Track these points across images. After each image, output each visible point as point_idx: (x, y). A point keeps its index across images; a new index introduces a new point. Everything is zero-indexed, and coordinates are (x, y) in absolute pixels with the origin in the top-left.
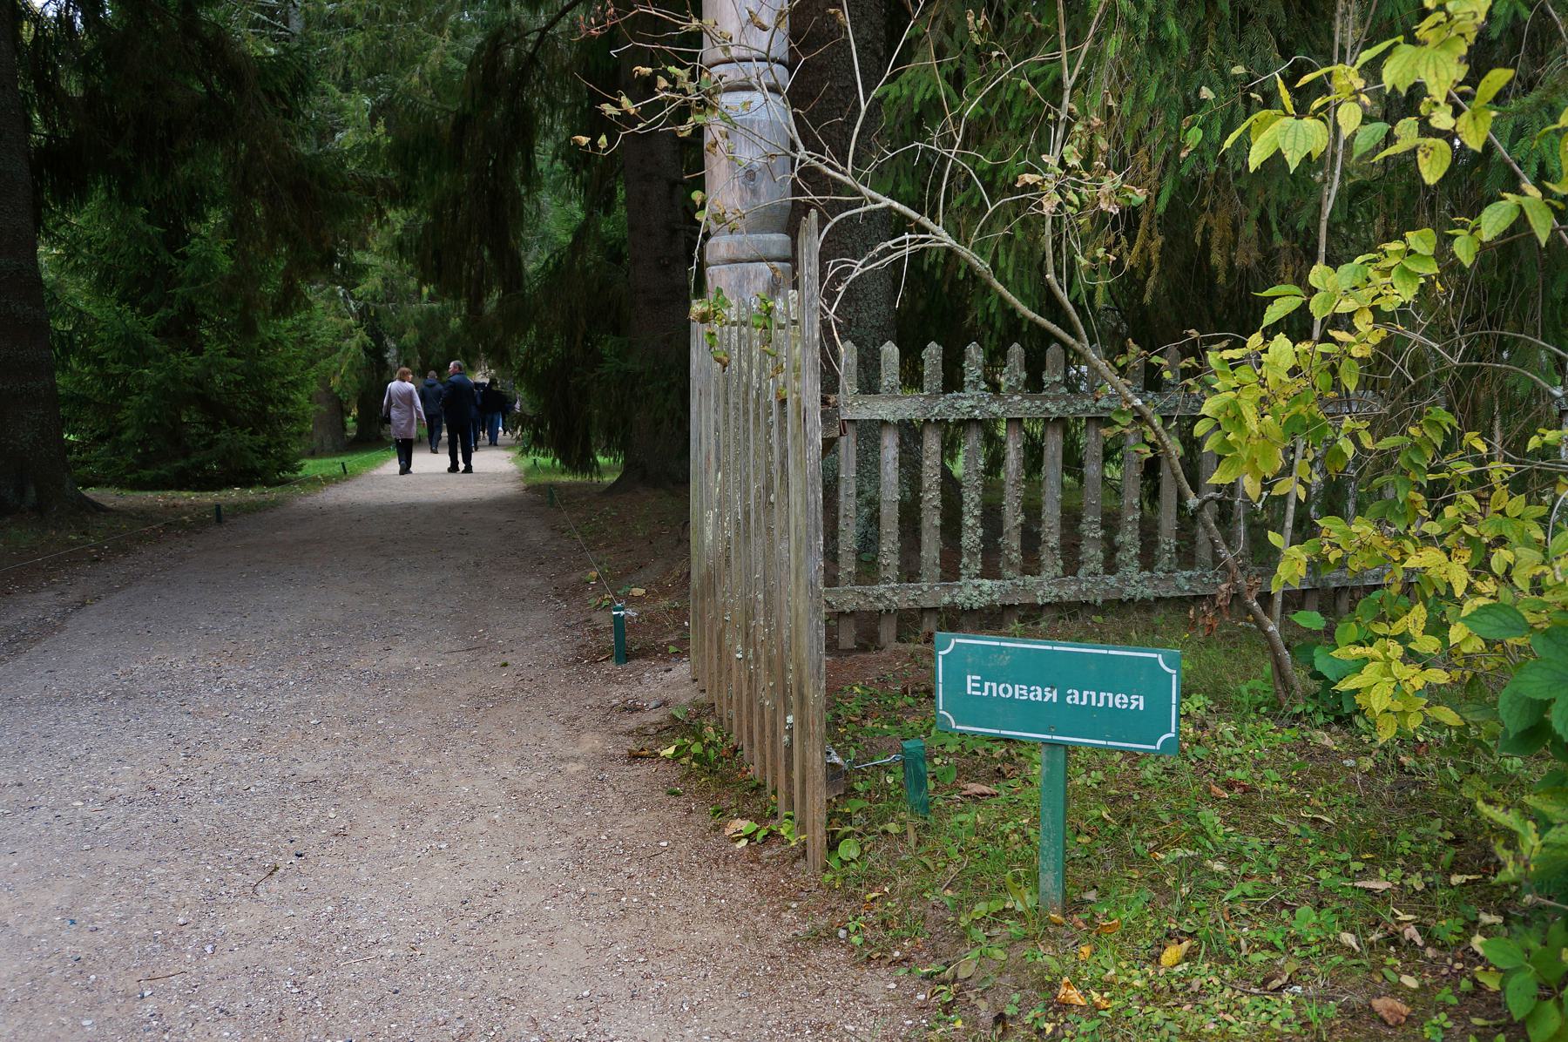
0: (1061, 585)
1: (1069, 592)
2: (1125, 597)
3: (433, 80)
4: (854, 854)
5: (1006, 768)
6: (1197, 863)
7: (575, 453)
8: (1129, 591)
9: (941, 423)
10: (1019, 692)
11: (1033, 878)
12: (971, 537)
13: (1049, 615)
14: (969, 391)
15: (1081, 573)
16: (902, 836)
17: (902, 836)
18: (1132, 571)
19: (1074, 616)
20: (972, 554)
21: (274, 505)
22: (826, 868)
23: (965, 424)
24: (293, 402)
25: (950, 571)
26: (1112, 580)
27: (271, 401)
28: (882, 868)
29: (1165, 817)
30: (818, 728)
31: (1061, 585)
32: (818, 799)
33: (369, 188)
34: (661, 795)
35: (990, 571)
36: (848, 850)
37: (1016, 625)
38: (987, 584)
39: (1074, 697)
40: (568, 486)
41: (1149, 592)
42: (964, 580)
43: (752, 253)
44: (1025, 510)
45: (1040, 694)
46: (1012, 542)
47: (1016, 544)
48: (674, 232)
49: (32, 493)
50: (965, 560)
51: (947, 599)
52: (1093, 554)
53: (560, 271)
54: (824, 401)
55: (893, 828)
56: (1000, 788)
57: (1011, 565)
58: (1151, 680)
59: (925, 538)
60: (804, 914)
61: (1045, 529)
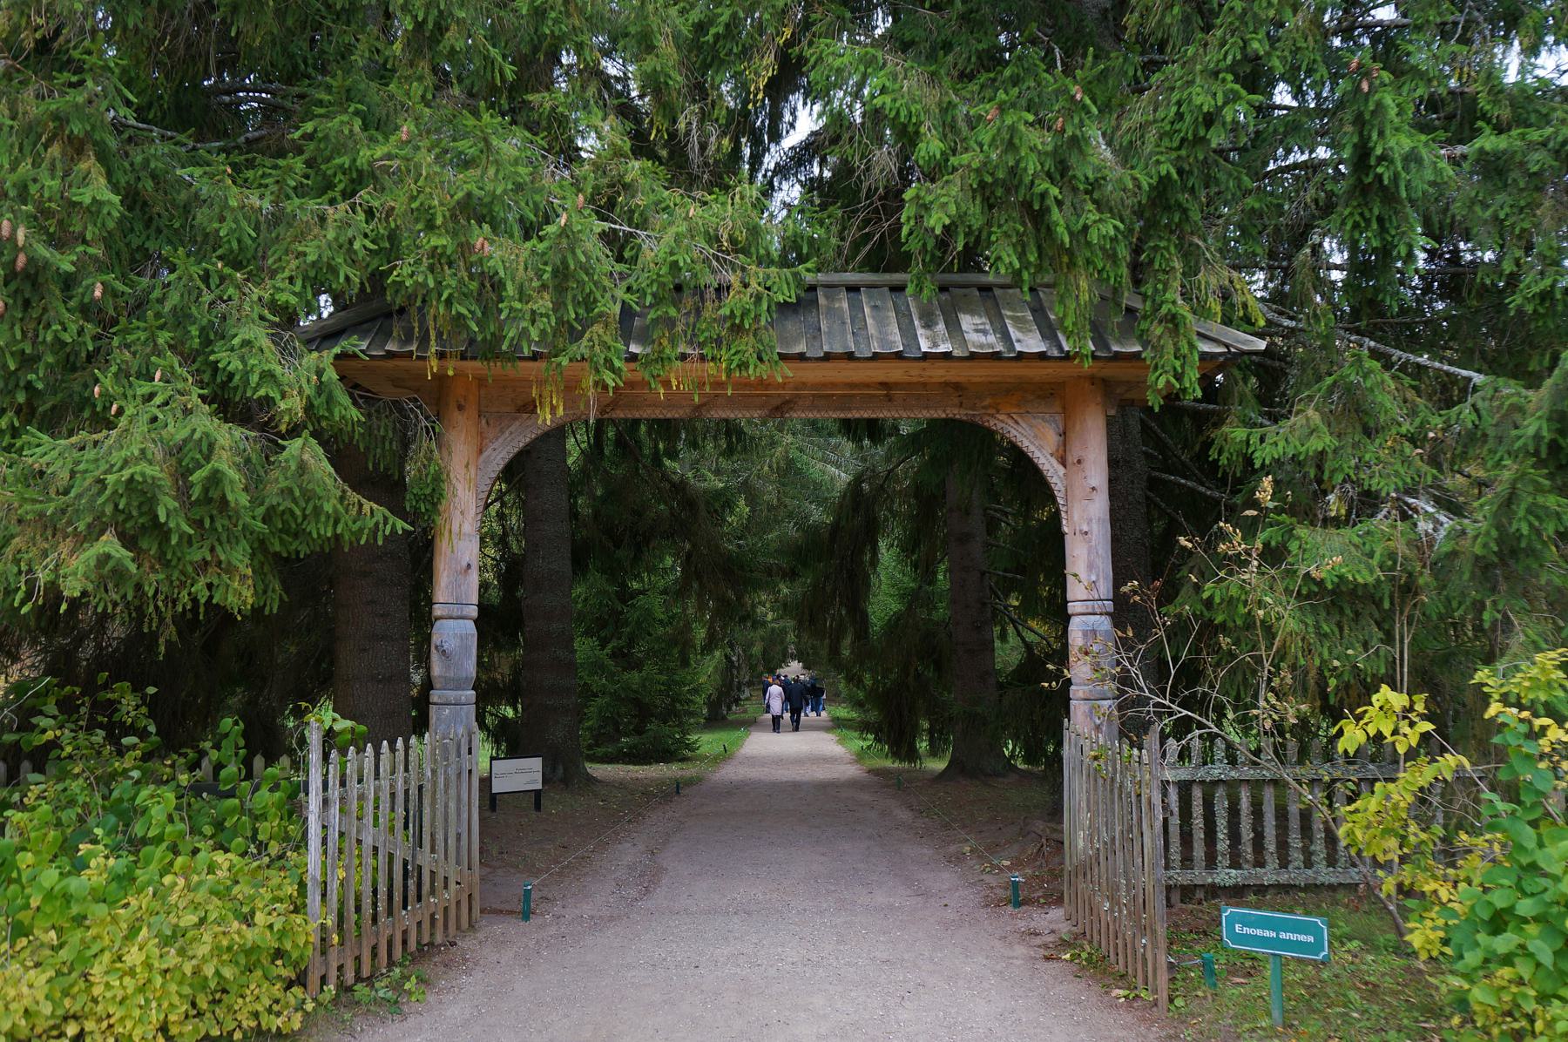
0: (1278, 874)
1: (1284, 878)
2: (1318, 882)
3: (778, 468)
4: (1182, 1004)
5: (1252, 972)
6: (1347, 1014)
7: (901, 745)
8: (1319, 881)
9: (1202, 782)
10: (1259, 932)
11: (1269, 1014)
12: (1223, 845)
13: (1272, 891)
14: (1218, 764)
15: (1290, 867)
16: (1205, 998)
17: (1205, 998)
18: (1322, 867)
19: (1287, 893)
20: (1223, 855)
21: (691, 782)
22: (1169, 1010)
23: (1217, 783)
24: (695, 703)
25: (1211, 862)
26: (1309, 872)
27: (680, 702)
28: (1197, 1010)
29: (1332, 995)
30: (1163, 945)
31: (1278, 874)
32: (1163, 978)
33: (769, 571)
34: (1071, 977)
35: (1235, 864)
36: (1179, 1002)
37: (1252, 898)
38: (1233, 872)
39: (1283, 935)
40: (898, 769)
41: (1333, 880)
42: (1219, 869)
43: (1098, 696)
44: (1254, 830)
45: (1267, 934)
46: (1247, 849)
47: (1249, 850)
48: (984, 604)
49: (560, 770)
50: (1220, 858)
51: (1210, 880)
52: (1297, 857)
53: (895, 625)
54: (1163, 801)
55: (1200, 993)
56: (1251, 980)
57: (1247, 861)
58: (1316, 932)
59: (1195, 845)
60: (1162, 1028)
61: (1266, 841)
